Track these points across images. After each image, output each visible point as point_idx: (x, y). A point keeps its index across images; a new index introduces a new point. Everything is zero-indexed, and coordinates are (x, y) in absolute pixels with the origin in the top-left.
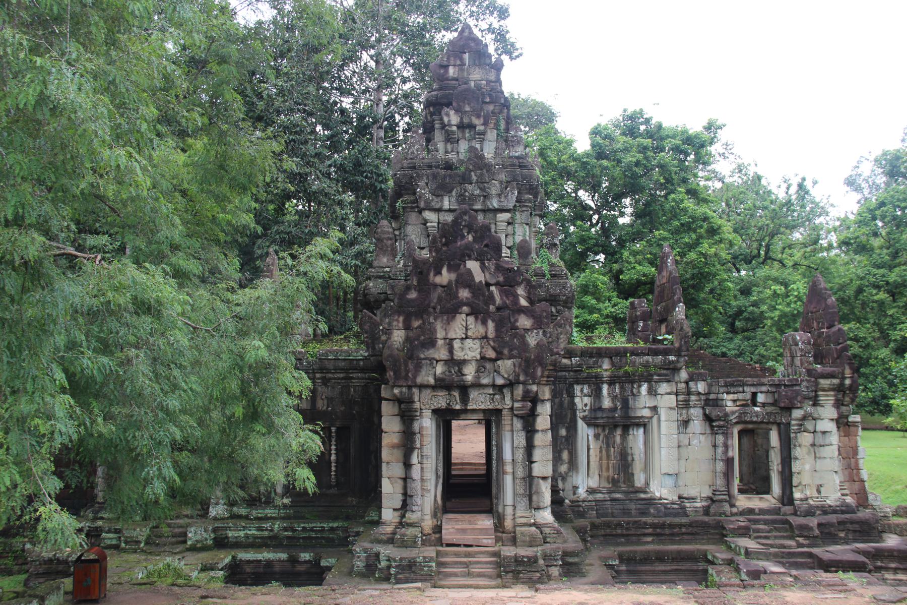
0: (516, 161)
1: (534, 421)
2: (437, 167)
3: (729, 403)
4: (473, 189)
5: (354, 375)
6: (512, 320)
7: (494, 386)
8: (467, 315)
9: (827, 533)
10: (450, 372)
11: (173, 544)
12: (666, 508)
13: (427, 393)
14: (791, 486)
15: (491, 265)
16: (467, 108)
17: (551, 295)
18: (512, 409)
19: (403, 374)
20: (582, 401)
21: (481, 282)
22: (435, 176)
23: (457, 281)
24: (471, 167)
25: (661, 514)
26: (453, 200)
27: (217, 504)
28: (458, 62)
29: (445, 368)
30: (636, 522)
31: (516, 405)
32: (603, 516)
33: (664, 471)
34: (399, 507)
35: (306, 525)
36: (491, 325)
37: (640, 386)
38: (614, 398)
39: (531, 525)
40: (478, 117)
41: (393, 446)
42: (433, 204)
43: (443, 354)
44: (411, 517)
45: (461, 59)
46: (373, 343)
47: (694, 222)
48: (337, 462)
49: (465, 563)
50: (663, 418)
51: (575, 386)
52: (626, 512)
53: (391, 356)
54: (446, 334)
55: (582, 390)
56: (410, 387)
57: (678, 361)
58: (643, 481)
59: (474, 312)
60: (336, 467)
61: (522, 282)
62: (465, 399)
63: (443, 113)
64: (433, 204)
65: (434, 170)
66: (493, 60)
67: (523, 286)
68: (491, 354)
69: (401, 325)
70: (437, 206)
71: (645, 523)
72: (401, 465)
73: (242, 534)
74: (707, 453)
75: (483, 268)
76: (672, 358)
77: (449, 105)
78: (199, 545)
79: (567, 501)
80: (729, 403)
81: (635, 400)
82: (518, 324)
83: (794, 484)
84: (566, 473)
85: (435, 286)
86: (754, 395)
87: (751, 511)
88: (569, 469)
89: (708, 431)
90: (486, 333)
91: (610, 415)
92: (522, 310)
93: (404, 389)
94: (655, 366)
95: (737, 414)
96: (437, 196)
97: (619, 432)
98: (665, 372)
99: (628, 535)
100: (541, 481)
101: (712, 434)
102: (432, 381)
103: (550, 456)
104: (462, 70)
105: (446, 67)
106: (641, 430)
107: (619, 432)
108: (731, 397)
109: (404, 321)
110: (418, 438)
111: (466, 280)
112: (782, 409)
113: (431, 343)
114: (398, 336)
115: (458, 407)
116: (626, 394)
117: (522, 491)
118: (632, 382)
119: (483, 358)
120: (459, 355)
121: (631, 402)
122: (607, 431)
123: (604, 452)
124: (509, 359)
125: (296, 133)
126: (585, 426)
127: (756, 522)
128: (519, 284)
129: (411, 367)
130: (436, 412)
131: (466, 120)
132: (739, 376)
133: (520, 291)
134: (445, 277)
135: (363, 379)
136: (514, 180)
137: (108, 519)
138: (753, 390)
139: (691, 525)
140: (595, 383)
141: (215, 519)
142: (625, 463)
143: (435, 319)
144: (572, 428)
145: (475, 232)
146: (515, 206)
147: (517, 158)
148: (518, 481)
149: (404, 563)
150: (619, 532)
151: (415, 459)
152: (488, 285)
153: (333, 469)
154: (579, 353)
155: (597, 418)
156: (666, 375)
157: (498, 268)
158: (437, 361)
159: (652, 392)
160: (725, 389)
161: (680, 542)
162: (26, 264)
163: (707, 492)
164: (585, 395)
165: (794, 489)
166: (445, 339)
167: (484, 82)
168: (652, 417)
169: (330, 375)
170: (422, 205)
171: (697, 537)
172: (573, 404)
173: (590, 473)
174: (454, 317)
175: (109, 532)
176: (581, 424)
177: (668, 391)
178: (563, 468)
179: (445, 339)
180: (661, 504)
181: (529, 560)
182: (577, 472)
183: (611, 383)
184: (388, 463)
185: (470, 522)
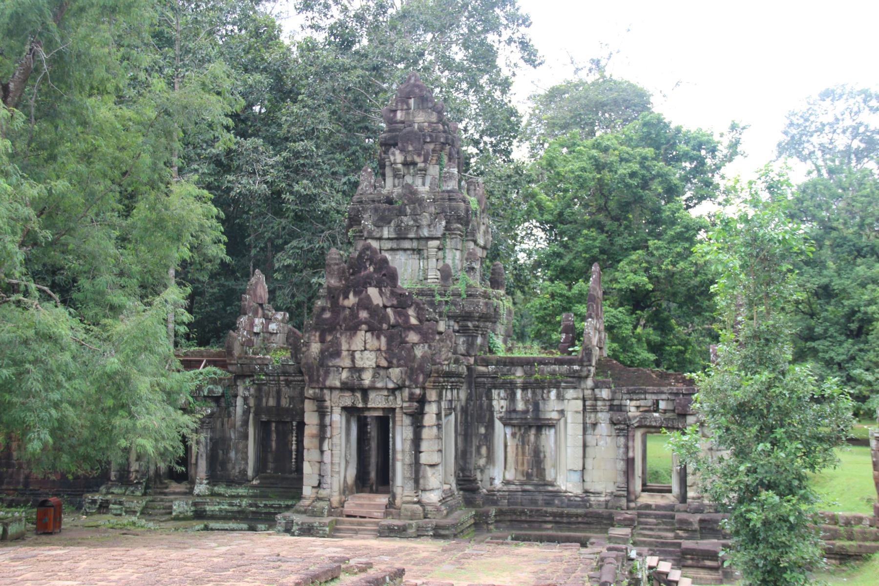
0: (446, 195)
1: (422, 418)
2: (379, 202)
3: (632, 409)
4: (407, 220)
6: (403, 335)
7: (388, 389)
8: (366, 332)
9: (710, 529)
11: (162, 514)
13: (336, 393)
14: (686, 486)
16: (410, 148)
17: (466, 312)
18: (402, 408)
19: (315, 378)
20: (499, 403)
22: (376, 210)
23: (358, 304)
24: (406, 202)
25: (564, 505)
26: (392, 230)
27: (201, 484)
28: (405, 107)
29: (349, 374)
30: (538, 510)
31: (405, 405)
32: (513, 505)
33: (569, 467)
35: (267, 502)
36: (383, 339)
37: (549, 392)
38: (526, 402)
40: (419, 155)
41: (313, 436)
42: (374, 234)
43: (347, 363)
44: (323, 493)
45: (408, 104)
46: (296, 353)
47: (687, 232)
49: (355, 530)
50: (569, 420)
51: (493, 391)
52: (534, 502)
53: (306, 364)
55: (499, 394)
56: (322, 389)
57: (581, 370)
59: (371, 329)
61: (411, 305)
62: (365, 398)
63: (390, 152)
64: (374, 234)
65: (376, 204)
67: (413, 308)
68: (384, 363)
69: (317, 339)
70: (378, 236)
71: (546, 512)
72: (318, 451)
73: (217, 508)
75: (381, 293)
76: (576, 367)
77: (395, 145)
78: (181, 516)
80: (633, 409)
81: (545, 404)
82: (407, 339)
83: (689, 483)
84: (484, 466)
85: (344, 308)
86: (656, 403)
87: (648, 507)
88: (487, 463)
91: (523, 416)
92: (412, 328)
93: (317, 391)
94: (561, 374)
95: (638, 419)
96: (378, 227)
97: (533, 431)
98: (571, 379)
99: (531, 522)
100: (428, 468)
102: (338, 384)
104: (408, 114)
105: (395, 111)
106: (552, 431)
107: (533, 431)
108: (634, 403)
109: (320, 336)
110: (328, 429)
111: (365, 304)
112: (679, 415)
113: (337, 354)
114: (315, 348)
115: (360, 405)
116: (537, 398)
117: (408, 475)
118: (543, 388)
119: (378, 366)
120: (359, 364)
121: (541, 405)
122: (522, 431)
123: (520, 449)
124: (398, 367)
125: (306, 157)
126: (502, 426)
127: (648, 516)
128: (410, 306)
129: (322, 372)
130: (344, 409)
131: (409, 159)
132: (643, 384)
133: (411, 312)
134: (352, 300)
136: (443, 211)
137: (118, 494)
138: (655, 397)
139: (586, 515)
141: (198, 495)
142: (538, 459)
143: (341, 335)
145: (375, 264)
146: (444, 234)
147: (448, 192)
148: (406, 467)
149: (305, 527)
150: (523, 518)
151: (326, 447)
153: (294, 456)
154: (494, 362)
155: (511, 419)
156: (572, 383)
157: (393, 293)
158: (343, 369)
159: (560, 397)
160: (628, 396)
161: (575, 530)
162: (338, 144)
163: (611, 488)
165: (688, 489)
166: (348, 351)
167: (426, 124)
168: (559, 420)
169: (291, 378)
170: (365, 234)
171: (592, 526)
172: (491, 406)
173: (508, 467)
174: (355, 333)
175: (115, 503)
176: (498, 425)
177: (575, 396)
179: (348, 351)
181: (399, 529)
182: (494, 465)
183: (524, 389)
184: (308, 449)
185: (370, 499)
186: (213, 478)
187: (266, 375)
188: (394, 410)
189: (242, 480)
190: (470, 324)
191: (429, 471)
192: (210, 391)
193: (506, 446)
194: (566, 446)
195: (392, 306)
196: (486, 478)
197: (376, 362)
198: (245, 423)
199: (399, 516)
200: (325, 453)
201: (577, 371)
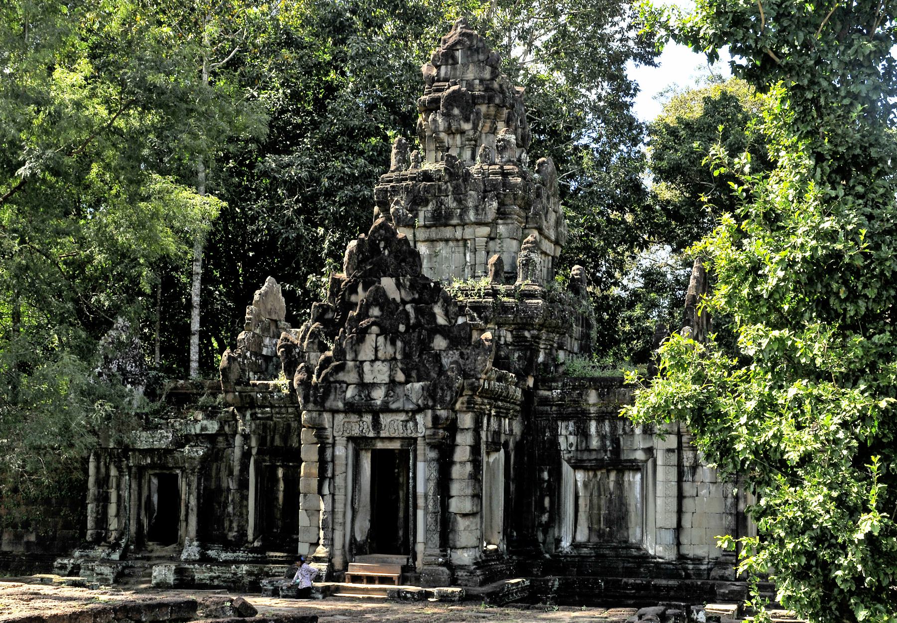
7: (407, 412)
8: (378, 335)
10: (360, 396)
13: (340, 417)
15: (406, 281)
28: (450, 61)
33: (658, 525)
36: (399, 344)
38: (603, 437)
39: (440, 565)
40: (467, 120)
50: (659, 462)
54: (356, 355)
62: (376, 425)
74: (717, 507)
75: (399, 285)
90: (395, 353)
100: (459, 518)
102: (341, 405)
106: (638, 476)
120: (368, 379)
124: (418, 381)
130: (350, 439)
140: (581, 418)
152: (404, 302)
168: (646, 461)
186: (205, 538)
187: (272, 406)
189: (240, 542)
190: (527, 334)
191: (462, 523)
192: (204, 428)
194: (655, 496)
195: (412, 301)
197: (390, 376)
199: (417, 581)
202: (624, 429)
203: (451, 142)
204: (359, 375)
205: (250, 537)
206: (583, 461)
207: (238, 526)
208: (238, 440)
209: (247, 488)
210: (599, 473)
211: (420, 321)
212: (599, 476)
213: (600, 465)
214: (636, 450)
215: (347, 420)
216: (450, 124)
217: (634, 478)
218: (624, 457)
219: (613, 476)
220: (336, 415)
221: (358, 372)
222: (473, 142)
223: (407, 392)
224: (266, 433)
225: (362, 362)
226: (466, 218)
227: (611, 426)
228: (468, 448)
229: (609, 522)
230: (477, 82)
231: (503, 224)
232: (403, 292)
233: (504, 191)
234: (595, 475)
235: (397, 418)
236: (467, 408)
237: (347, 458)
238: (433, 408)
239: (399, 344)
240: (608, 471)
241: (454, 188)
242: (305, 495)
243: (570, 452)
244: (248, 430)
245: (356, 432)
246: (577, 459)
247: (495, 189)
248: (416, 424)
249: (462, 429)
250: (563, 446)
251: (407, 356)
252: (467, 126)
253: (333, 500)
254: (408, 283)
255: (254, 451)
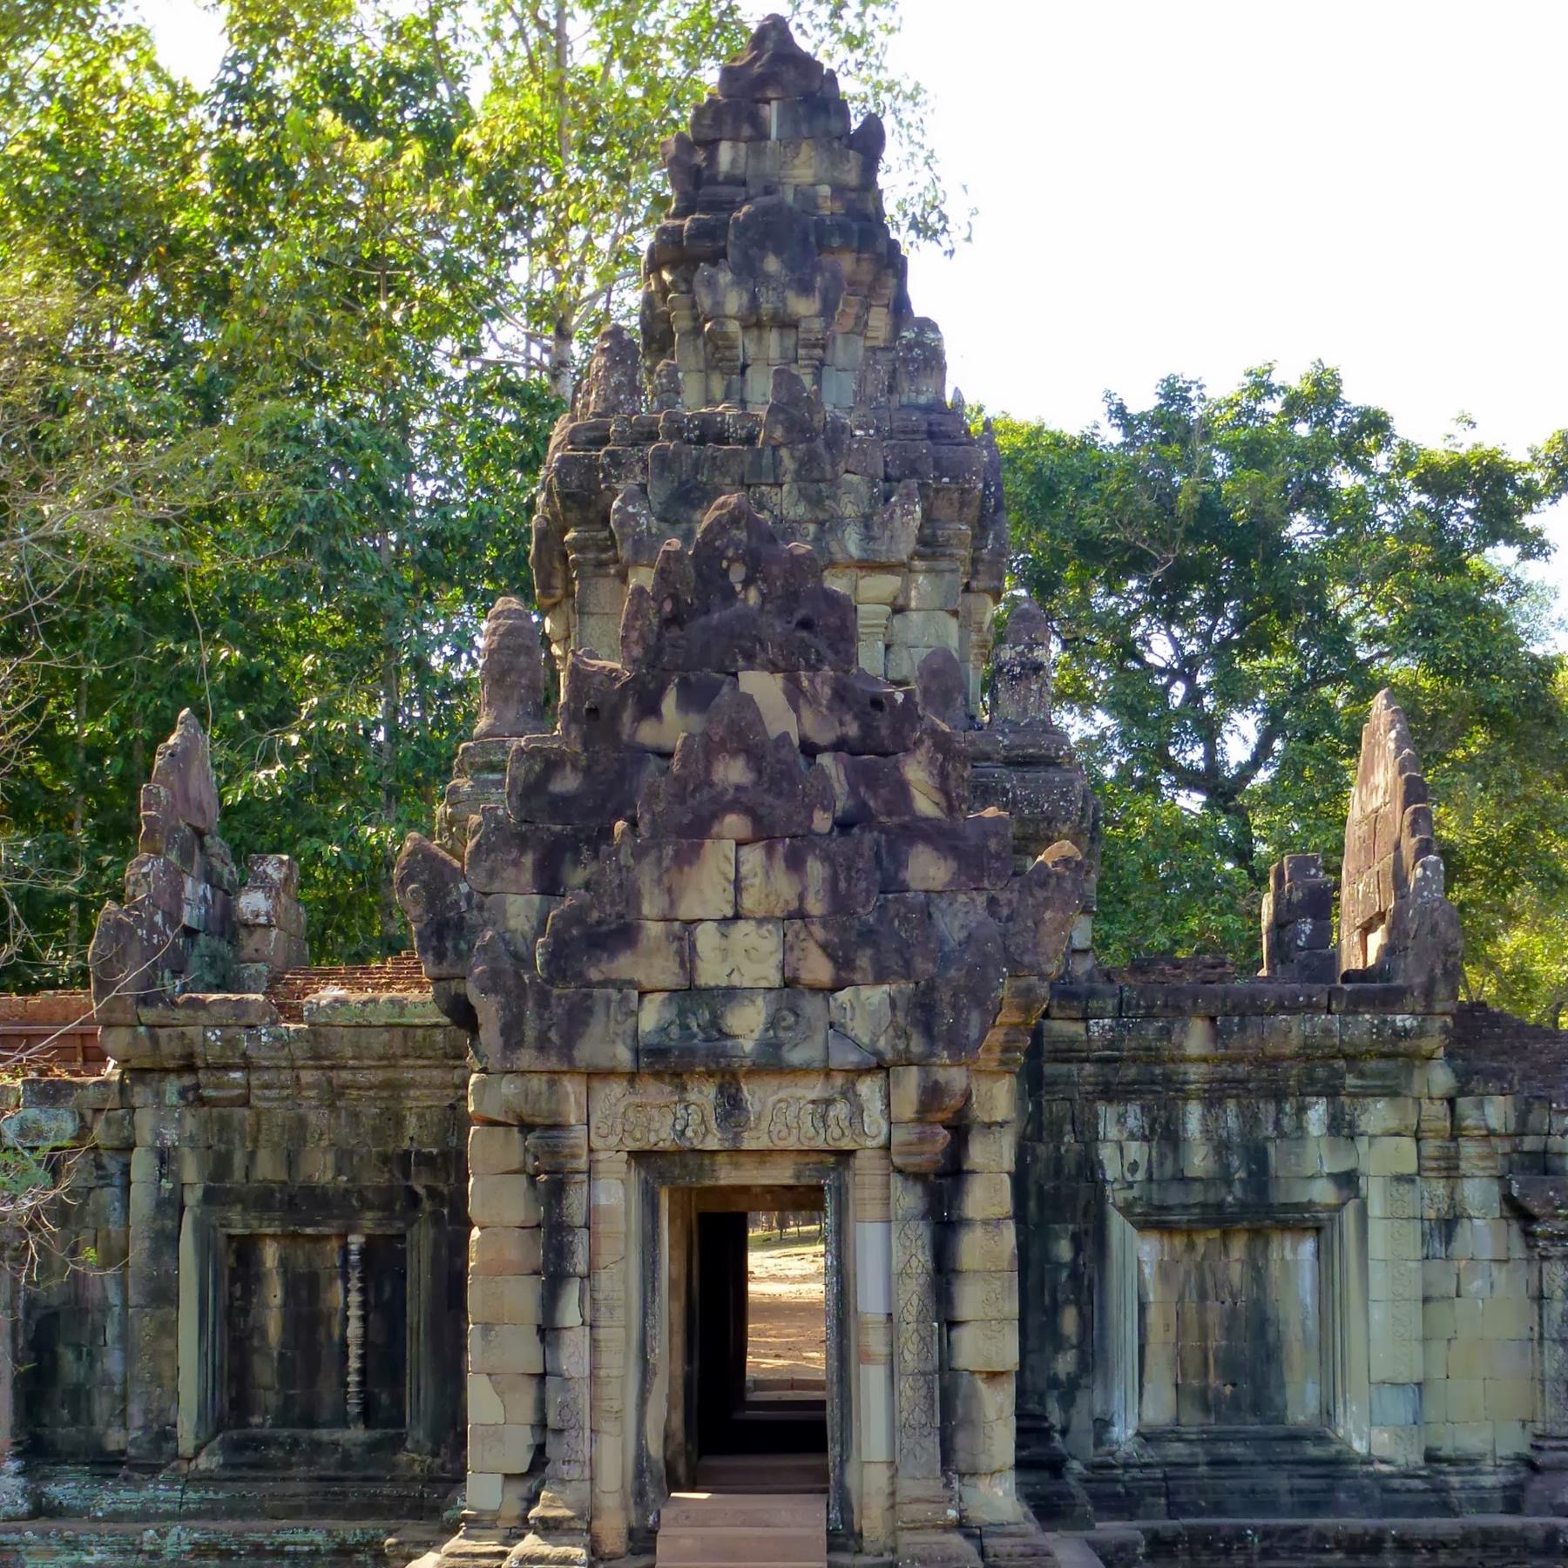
5: (417, 1076)
12: (1385, 1490)
15: (821, 684)
21: (785, 736)
28: (746, 131)
29: (670, 1014)
34: (525, 1469)
36: (816, 869)
37: (1302, 1110)
38: (1221, 1148)
39: (947, 1528)
40: (805, 288)
48: (365, 1343)
50: (1375, 1209)
54: (673, 904)
58: (1312, 1405)
59: (763, 833)
60: (362, 1357)
62: (731, 1107)
66: (855, 125)
67: (921, 754)
69: (527, 877)
71: (1321, 1536)
75: (795, 694)
77: (716, 258)
79: (1076, 1466)
89: (1518, 1250)
90: (801, 897)
100: (982, 1386)
101: (1529, 1260)
103: (1012, 1307)
106: (1308, 1247)
110: (580, 1244)
115: (712, 1143)
117: (919, 1417)
118: (1279, 1096)
120: (711, 973)
124: (879, 979)
135: (444, 1086)
144: (1094, 1240)
148: (905, 1385)
151: (570, 1313)
152: (810, 750)
156: (1383, 1075)
157: (842, 695)
159: (1342, 1128)
163: (1515, 1442)
164: (1132, 1137)
168: (1338, 1208)
169: (346, 1076)
172: (1090, 1167)
176: (1118, 1226)
177: (1393, 1124)
178: (1065, 1364)
180: (1368, 1475)
183: (1213, 1100)
188: (844, 1156)
193: (1142, 1308)
195: (839, 746)
196: (1081, 1421)
198: (167, 1241)
200: (567, 1337)
201: (1407, 1032)
202: (1277, 1124)
203: (752, 350)
204: (682, 964)
205: (186, 1443)
206: (1163, 1208)
207: (146, 1412)
208: (142, 1165)
209: (174, 1302)
210: (1200, 1241)
211: (864, 804)
212: (1201, 1249)
213: (1219, 1219)
214: (1312, 1177)
215: (637, 1100)
216: (754, 299)
217: (1295, 1250)
218: (1278, 1196)
219: (1238, 1247)
220: (596, 1084)
221: (680, 953)
222: (818, 352)
223: (836, 1016)
224: (229, 1142)
225: (691, 924)
226: (834, 547)
227: (1241, 1114)
228: (1007, 1179)
229: (1231, 1368)
230: (825, 190)
231: (928, 571)
232: (807, 714)
233: (937, 479)
234: (1191, 1246)
235: (799, 1092)
236: (1002, 1063)
237: (627, 1213)
238: (923, 1062)
239: (816, 869)
240: (1226, 1234)
241: (802, 464)
242: (487, 1327)
243: (1130, 1186)
244: (171, 1136)
245: (662, 1135)
246: (1150, 1204)
247: (914, 472)
248: (858, 1111)
249: (989, 1126)
250: (1112, 1170)
251: (840, 903)
252: (804, 307)
253: (594, 1343)
254: (827, 691)
255: (192, 1197)
